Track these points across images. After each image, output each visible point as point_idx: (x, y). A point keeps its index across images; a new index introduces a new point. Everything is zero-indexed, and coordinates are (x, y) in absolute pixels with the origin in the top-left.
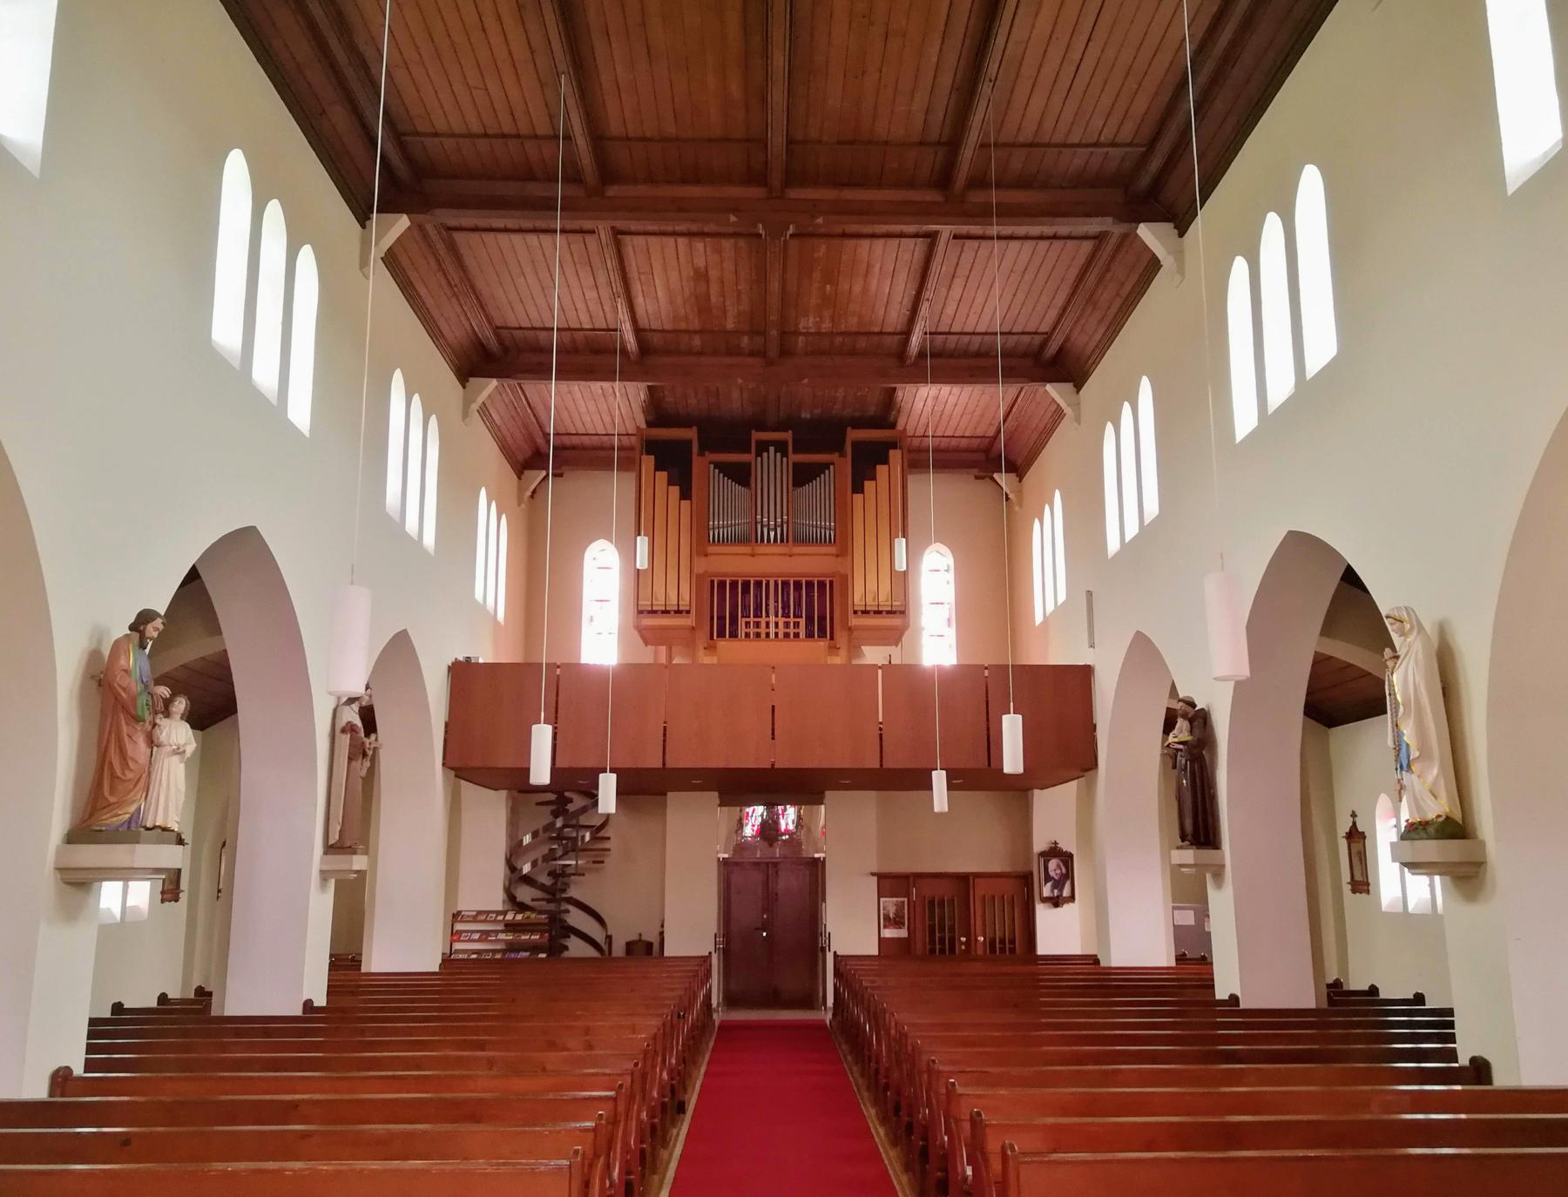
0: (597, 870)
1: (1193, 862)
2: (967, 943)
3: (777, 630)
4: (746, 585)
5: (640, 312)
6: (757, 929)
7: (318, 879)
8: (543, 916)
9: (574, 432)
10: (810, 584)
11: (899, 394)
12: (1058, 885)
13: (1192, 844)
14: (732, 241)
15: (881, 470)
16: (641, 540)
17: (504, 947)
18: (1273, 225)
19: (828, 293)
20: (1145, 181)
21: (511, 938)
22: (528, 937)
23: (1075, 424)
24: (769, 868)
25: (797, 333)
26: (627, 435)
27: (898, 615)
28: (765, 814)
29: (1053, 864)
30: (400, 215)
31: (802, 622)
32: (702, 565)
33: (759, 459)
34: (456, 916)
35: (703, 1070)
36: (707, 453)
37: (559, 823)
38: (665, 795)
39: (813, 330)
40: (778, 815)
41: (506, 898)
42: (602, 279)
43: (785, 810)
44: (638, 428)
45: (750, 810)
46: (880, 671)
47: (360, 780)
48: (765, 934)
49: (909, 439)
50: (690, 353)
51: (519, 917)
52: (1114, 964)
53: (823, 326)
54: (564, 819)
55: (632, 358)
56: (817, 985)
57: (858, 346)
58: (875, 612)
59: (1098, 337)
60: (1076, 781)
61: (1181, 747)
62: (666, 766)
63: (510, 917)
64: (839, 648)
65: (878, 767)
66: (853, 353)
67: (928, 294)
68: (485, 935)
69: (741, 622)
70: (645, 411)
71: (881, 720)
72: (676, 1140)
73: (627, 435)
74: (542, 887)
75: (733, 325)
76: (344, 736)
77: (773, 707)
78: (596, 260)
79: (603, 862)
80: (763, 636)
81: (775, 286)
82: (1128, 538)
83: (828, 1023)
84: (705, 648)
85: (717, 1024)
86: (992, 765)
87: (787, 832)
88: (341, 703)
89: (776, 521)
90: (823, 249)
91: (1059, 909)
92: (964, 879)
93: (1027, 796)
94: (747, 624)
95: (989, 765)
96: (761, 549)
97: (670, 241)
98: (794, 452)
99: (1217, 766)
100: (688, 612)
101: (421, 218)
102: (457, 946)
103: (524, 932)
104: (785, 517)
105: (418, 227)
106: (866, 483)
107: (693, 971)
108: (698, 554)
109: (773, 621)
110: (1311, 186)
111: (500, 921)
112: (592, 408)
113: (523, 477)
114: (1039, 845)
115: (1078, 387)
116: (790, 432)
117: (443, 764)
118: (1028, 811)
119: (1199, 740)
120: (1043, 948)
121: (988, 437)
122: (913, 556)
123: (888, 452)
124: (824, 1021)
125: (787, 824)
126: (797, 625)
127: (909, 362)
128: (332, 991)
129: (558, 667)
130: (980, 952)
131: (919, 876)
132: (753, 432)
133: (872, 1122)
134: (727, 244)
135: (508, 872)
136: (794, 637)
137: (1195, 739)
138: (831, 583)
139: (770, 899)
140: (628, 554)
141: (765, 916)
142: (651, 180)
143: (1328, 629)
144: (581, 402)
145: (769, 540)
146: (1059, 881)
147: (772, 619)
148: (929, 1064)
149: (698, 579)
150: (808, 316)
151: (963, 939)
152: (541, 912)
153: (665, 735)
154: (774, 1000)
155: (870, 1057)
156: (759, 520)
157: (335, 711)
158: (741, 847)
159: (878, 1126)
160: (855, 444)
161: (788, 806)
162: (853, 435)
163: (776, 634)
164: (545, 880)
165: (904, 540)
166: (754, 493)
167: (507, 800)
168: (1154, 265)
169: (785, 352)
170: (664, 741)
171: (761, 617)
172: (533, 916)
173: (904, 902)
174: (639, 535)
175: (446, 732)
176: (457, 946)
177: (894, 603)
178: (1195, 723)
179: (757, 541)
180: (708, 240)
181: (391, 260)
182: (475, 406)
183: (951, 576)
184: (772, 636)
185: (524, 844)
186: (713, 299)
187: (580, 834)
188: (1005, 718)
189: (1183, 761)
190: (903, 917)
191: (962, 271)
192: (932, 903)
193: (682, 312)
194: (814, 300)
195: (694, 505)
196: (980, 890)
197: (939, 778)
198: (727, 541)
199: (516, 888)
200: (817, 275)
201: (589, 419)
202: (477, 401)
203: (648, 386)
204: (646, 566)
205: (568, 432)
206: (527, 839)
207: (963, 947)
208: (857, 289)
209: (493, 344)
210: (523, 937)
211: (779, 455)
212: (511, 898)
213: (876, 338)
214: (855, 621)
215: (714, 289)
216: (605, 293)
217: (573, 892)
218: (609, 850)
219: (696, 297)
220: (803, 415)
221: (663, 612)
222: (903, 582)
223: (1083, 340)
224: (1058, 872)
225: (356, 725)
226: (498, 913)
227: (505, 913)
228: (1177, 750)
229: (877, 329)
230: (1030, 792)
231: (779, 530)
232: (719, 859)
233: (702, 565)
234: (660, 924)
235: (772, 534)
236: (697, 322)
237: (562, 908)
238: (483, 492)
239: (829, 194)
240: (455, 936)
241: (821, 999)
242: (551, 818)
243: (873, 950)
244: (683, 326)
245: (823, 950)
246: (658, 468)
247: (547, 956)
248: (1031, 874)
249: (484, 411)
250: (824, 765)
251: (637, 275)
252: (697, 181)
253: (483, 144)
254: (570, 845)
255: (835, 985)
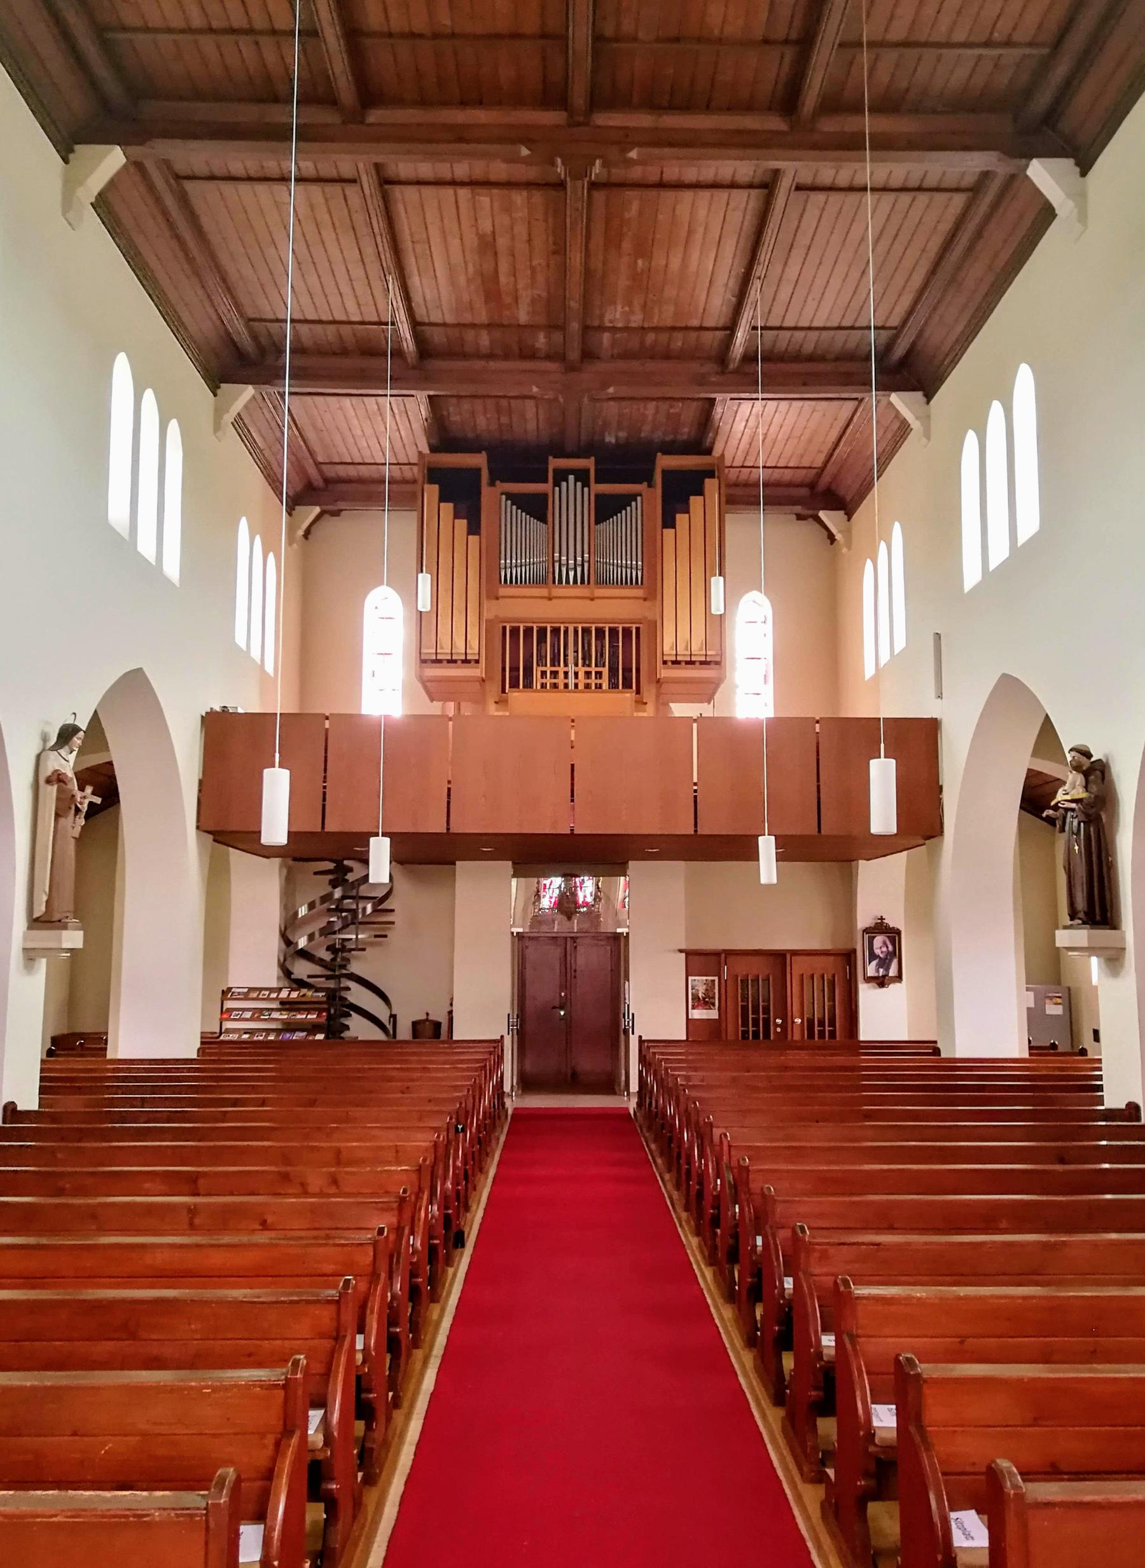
0: (379, 944)
1: (1085, 944)
2: (784, 1026)
3: (577, 681)
4: (542, 632)
5: (417, 298)
6: (554, 1007)
7: (21, 958)
8: (321, 994)
9: (349, 461)
10: (613, 632)
11: (718, 410)
12: (884, 963)
13: (1084, 923)
14: (525, 193)
15: (695, 501)
16: (424, 579)
17: (280, 1027)
18: (996, 409)
19: (639, 270)
20: (1043, 100)
21: (286, 1017)
22: (304, 1016)
23: (924, 440)
24: (567, 944)
25: (601, 328)
26: (410, 464)
27: (713, 666)
28: (563, 886)
29: (879, 940)
30: (108, 147)
31: (605, 671)
32: (493, 610)
33: (557, 489)
34: (226, 993)
35: (492, 1172)
36: (498, 482)
37: (338, 893)
38: (455, 864)
39: (620, 325)
40: (576, 887)
41: (281, 974)
42: (369, 251)
43: (583, 882)
44: (420, 453)
45: (547, 882)
46: (695, 725)
47: (73, 841)
48: (562, 1013)
49: (726, 470)
50: (478, 355)
51: (294, 995)
52: (959, 1055)
53: (633, 318)
54: (344, 891)
55: (409, 360)
56: (617, 1067)
57: (672, 347)
58: (687, 663)
59: (960, 328)
60: (905, 853)
61: (1073, 805)
62: (451, 831)
63: (284, 994)
64: (646, 703)
65: (693, 833)
66: (667, 356)
67: (759, 270)
68: (258, 1013)
69: (537, 671)
70: (428, 432)
71: (695, 780)
72: (452, 1284)
73: (410, 464)
74: (320, 962)
75: (527, 318)
76: (49, 787)
77: (573, 766)
78: (363, 230)
79: (386, 936)
80: (561, 687)
81: (576, 259)
82: (897, 651)
83: (632, 1112)
84: (496, 703)
85: (510, 1112)
86: (822, 832)
87: (586, 904)
88: (48, 747)
89: (575, 560)
90: (635, 206)
91: (884, 989)
92: (780, 958)
93: (851, 868)
94: (544, 674)
95: (819, 831)
96: (558, 591)
97: (449, 191)
98: (596, 482)
99: (1118, 825)
100: (477, 661)
101: (137, 151)
102: (228, 1025)
103: (299, 1010)
104: (586, 555)
105: (136, 166)
106: (678, 516)
107: (477, 1061)
108: (488, 597)
109: (573, 669)
110: (1025, 380)
111: (273, 999)
112: (369, 431)
113: (219, 391)
114: (864, 920)
115: (929, 397)
116: (593, 458)
117: (198, 827)
118: (851, 887)
119: (1096, 797)
120: (866, 1033)
121: (891, 328)
122: (731, 599)
123: (703, 483)
124: (627, 1109)
125: (585, 897)
126: (599, 675)
127: (731, 366)
128: (47, 1087)
129: (327, 718)
130: (797, 1037)
131: (729, 953)
132: (551, 458)
133: (694, 1255)
134: (519, 198)
135: (284, 946)
136: (596, 688)
137: (1093, 796)
138: (638, 629)
139: (568, 975)
140: (410, 594)
141: (563, 994)
142: (423, 102)
143: (1036, 753)
144: (355, 422)
145: (568, 582)
146: (886, 959)
147: (571, 669)
148: (739, 1161)
149: (489, 627)
150: (615, 304)
151: (779, 1021)
152: (317, 990)
153: (449, 795)
154: (574, 1083)
155: (688, 1172)
156: (557, 558)
157: (38, 757)
158: (537, 920)
159: (703, 1266)
160: (665, 472)
161: (586, 878)
162: (665, 462)
163: (576, 686)
164: (327, 956)
165: (721, 579)
166: (551, 529)
167: (280, 870)
168: (1046, 214)
169: (589, 355)
170: (449, 803)
171: (559, 665)
172: (310, 993)
173: (714, 981)
174: (422, 572)
175: (200, 791)
176: (228, 1025)
177: (708, 653)
178: (1092, 777)
179: (554, 582)
180: (495, 191)
181: (103, 204)
182: (229, 417)
183: (769, 628)
184: (571, 687)
185: (300, 916)
186: (503, 279)
187: (361, 906)
188: (874, 763)
189: (1075, 823)
190: (714, 998)
191: (803, 240)
192: (745, 982)
193: (466, 297)
194: (623, 282)
195: (483, 540)
196: (798, 967)
197: (767, 845)
198: (521, 582)
199: (293, 964)
200: (627, 245)
201: (365, 444)
202: (231, 410)
203: (429, 396)
204: (428, 608)
205: (344, 461)
206: (303, 911)
207: (779, 1030)
208: (675, 263)
209: (318, 482)
210: (299, 1016)
211: (579, 484)
212: (287, 973)
213: (693, 335)
214: (664, 673)
215: (504, 267)
216: (374, 269)
217: (355, 968)
218: (393, 923)
219: (482, 275)
220: (607, 439)
221: (449, 661)
222: (718, 625)
223: (939, 336)
224: (884, 949)
225: (64, 774)
226: (271, 990)
227: (280, 990)
228: (1067, 810)
229: (695, 323)
230: (854, 863)
231: (579, 569)
232: (513, 933)
233: (493, 610)
234: (449, 1002)
235: (571, 574)
236: (484, 313)
237: (342, 985)
238: (243, 525)
239: (644, 120)
240: (226, 1014)
241: (623, 1083)
242: (330, 889)
243: (679, 1033)
244: (467, 318)
245: (626, 1032)
246: (443, 498)
247: (327, 1037)
248: (854, 951)
249: (239, 423)
250: (631, 831)
251: (410, 244)
252: (480, 103)
253: (208, 43)
254: (350, 917)
255: (640, 1072)
